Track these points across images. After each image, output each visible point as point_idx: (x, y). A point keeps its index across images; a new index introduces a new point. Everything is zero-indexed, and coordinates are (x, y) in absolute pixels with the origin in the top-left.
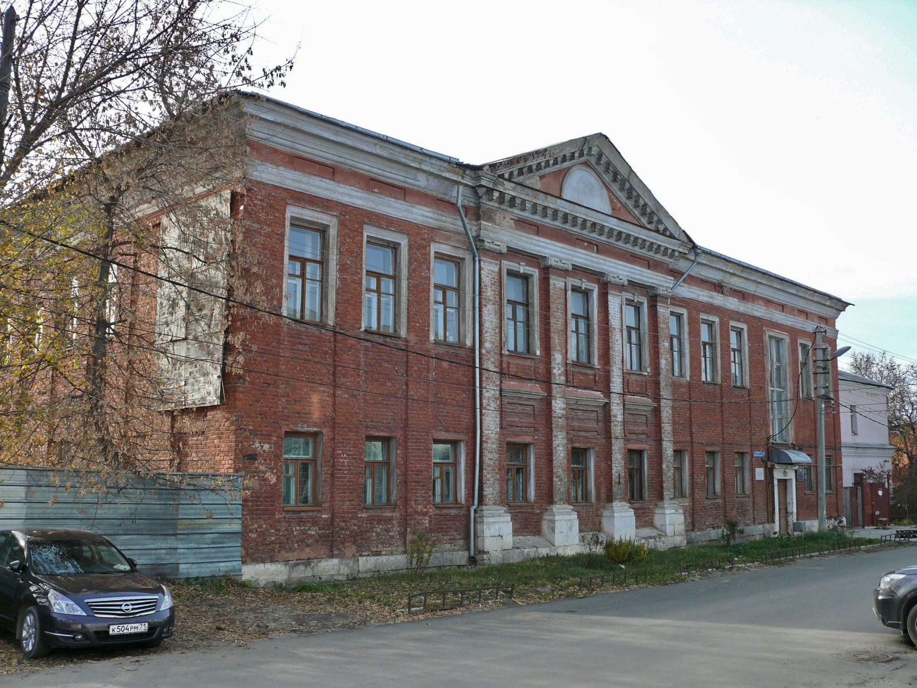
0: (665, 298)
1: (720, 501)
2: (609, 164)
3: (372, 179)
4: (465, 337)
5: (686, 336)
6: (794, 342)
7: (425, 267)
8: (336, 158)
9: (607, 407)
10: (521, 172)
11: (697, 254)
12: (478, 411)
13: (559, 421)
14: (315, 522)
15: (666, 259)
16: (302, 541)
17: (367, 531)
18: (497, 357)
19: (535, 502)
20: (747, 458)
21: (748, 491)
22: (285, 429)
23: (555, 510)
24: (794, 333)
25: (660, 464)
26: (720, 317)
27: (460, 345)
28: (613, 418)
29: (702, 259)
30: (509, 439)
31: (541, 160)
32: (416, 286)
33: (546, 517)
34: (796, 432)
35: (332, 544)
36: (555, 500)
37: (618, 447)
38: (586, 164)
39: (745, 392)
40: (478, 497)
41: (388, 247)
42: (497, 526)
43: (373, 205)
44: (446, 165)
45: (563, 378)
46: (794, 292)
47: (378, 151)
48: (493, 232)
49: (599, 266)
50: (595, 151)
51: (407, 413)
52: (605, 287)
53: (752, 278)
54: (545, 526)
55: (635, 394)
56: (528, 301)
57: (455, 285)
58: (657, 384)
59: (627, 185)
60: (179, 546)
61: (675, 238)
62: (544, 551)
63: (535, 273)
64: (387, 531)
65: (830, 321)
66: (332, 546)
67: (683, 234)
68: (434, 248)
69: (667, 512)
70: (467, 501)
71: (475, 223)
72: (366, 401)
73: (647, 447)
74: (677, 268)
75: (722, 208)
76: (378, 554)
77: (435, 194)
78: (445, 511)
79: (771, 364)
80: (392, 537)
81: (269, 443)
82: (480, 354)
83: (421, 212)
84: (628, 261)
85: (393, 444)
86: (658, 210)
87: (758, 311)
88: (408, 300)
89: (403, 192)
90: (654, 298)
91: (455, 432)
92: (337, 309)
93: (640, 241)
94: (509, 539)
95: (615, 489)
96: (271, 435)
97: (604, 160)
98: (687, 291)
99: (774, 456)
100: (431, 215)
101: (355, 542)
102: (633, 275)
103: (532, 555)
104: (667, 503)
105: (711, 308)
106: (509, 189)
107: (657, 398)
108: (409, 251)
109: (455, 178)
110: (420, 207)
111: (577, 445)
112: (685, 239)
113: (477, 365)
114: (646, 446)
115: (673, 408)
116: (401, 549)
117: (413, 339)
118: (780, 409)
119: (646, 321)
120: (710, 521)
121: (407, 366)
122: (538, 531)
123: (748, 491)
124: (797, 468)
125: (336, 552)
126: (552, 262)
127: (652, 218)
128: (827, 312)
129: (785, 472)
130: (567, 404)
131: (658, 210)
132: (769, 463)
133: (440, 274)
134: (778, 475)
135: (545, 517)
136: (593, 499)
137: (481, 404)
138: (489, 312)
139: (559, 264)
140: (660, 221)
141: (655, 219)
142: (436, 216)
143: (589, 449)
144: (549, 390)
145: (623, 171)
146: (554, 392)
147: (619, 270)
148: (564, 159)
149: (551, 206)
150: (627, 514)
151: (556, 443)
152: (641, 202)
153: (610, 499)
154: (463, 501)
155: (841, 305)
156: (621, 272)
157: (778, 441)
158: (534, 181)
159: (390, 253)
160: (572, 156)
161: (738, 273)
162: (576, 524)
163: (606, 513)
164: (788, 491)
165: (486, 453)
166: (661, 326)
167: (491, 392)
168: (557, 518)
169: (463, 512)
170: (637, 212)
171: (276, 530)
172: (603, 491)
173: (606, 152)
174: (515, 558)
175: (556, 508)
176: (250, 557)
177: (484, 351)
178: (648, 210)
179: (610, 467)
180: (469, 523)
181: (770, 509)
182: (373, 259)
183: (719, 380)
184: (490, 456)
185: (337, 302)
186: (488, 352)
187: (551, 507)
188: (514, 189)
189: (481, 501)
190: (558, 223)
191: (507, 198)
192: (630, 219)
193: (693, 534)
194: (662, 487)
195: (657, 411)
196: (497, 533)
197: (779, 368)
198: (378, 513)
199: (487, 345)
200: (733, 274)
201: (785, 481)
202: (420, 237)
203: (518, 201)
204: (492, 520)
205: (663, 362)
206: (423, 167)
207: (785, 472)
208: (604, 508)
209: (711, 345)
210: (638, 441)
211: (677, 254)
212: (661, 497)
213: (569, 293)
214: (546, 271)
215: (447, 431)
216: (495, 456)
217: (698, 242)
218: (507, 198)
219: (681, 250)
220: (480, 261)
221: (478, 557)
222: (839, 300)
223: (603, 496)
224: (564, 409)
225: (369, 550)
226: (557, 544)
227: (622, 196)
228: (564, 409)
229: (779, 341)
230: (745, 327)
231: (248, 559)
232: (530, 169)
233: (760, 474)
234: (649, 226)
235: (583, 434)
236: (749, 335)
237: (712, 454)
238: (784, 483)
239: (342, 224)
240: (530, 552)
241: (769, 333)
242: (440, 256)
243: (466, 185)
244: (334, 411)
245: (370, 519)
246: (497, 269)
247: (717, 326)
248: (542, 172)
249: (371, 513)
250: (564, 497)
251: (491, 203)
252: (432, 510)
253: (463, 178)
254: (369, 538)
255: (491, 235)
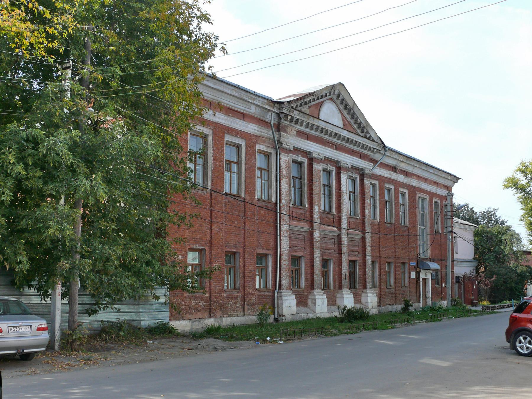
0: (368, 175)
1: (393, 290)
2: (343, 100)
3: (229, 109)
4: (272, 196)
5: (377, 197)
6: (431, 200)
7: (253, 158)
8: (212, 97)
9: (339, 236)
10: (301, 105)
11: (386, 151)
12: (279, 237)
13: (317, 244)
14: (202, 299)
15: (369, 153)
16: (196, 308)
17: (226, 304)
18: (288, 208)
19: (305, 289)
20: (407, 266)
21: (407, 285)
22: (188, 247)
23: (315, 293)
24: (432, 195)
25: (365, 268)
26: (394, 186)
27: (269, 201)
28: (342, 243)
29: (388, 153)
30: (292, 254)
31: (311, 98)
32: (249, 168)
33: (310, 297)
34: (432, 252)
35: (210, 311)
36: (315, 287)
37: (345, 259)
38: (331, 99)
39: (406, 229)
40: (277, 285)
41: (262, 154)
42: (289, 301)
43: (229, 124)
44: (266, 101)
45: (319, 220)
46: (432, 171)
47: (234, 93)
48: (286, 138)
49: (337, 157)
50: (337, 92)
51: (245, 239)
52: (339, 169)
53: (412, 164)
54: (310, 302)
55: (352, 229)
56: (301, 176)
57: (266, 168)
58: (364, 224)
59: (352, 112)
60: (141, 310)
61: (375, 142)
62: (311, 316)
63: (305, 161)
64: (235, 303)
65: (449, 188)
66: (210, 312)
67: (379, 139)
68: (259, 147)
69: (369, 295)
70: (272, 287)
71: (277, 133)
72: (225, 232)
73: (358, 259)
74: (374, 158)
75: (401, 125)
76: (231, 316)
77: (258, 116)
78: (262, 293)
79: (419, 212)
80: (238, 307)
81: (181, 255)
82: (280, 207)
83: (252, 127)
84: (350, 154)
85: (237, 256)
86: (367, 126)
87: (414, 182)
88: (245, 176)
89: (243, 116)
90: (363, 175)
91: (267, 249)
92: (212, 181)
93: (358, 143)
94: (294, 309)
95: (343, 282)
96: (181, 250)
97: (341, 98)
98: (380, 171)
99: (420, 265)
100: (259, 129)
101: (221, 310)
102: (353, 162)
103: (305, 318)
104: (368, 290)
105: (390, 181)
106: (296, 115)
107: (364, 232)
108: (246, 149)
109: (269, 108)
110: (251, 124)
111: (325, 257)
112: (380, 142)
113: (278, 211)
114: (358, 259)
115: (372, 237)
116: (242, 313)
117: (248, 198)
118: (423, 239)
119: (359, 188)
120: (388, 301)
121: (245, 213)
122: (306, 305)
123: (407, 285)
124: (432, 272)
125: (212, 315)
126: (315, 155)
127: (364, 130)
128: (448, 183)
129: (426, 274)
130: (321, 234)
131: (367, 126)
132: (418, 269)
133: (259, 161)
134: (422, 276)
135: (310, 297)
136: (332, 288)
137: (280, 234)
138: (284, 182)
139: (318, 156)
140: (367, 132)
141: (365, 130)
142: (259, 129)
143: (330, 259)
144: (312, 226)
145: (350, 104)
146: (315, 228)
147: (347, 160)
148: (322, 97)
149: (316, 124)
150: (349, 296)
151: (315, 256)
152: (359, 121)
153: (341, 287)
154: (270, 288)
155: (457, 179)
156: (347, 161)
157: (422, 257)
158: (306, 109)
159: (234, 149)
160: (326, 96)
161: (404, 161)
162: (326, 300)
163: (339, 295)
164: (427, 285)
165: (282, 261)
166: (366, 191)
167: (285, 227)
168: (317, 297)
169: (271, 294)
170: (355, 127)
171: (185, 303)
172: (337, 283)
173: (343, 93)
174: (298, 318)
175: (316, 292)
176: (173, 317)
177: (281, 205)
178: (362, 126)
179: (341, 270)
180: (274, 300)
181: (418, 295)
182: (229, 154)
183: (393, 221)
184: (284, 263)
185: (212, 177)
186: (283, 205)
187: (313, 291)
188: (298, 115)
189: (280, 288)
190: (318, 133)
191: (295, 119)
192: (352, 130)
193: (380, 308)
194: (366, 281)
195: (363, 239)
196: (289, 305)
197: (423, 215)
198: (231, 294)
199: (283, 201)
200: (402, 162)
201: (425, 279)
202: (251, 140)
203: (300, 121)
204: (286, 298)
205: (367, 211)
206: (255, 102)
207: (426, 274)
208: (338, 292)
209: (389, 202)
210: (354, 256)
211: (375, 150)
212: (365, 287)
213: (322, 172)
214: (311, 160)
215: (263, 249)
216: (287, 263)
217: (386, 144)
218: (295, 119)
219: (378, 148)
220: (280, 154)
221: (279, 318)
222: (455, 176)
223: (337, 286)
224: (319, 237)
225: (227, 314)
226: (316, 312)
227: (348, 117)
228: (319, 237)
229: (423, 200)
230: (406, 191)
231: (172, 319)
232: (306, 103)
233: (413, 275)
234: (361, 134)
235: (327, 251)
236: (409, 196)
237: (389, 263)
238: (425, 280)
239: (214, 134)
240: (304, 316)
241: (419, 195)
242: (260, 152)
243: (274, 112)
244: (211, 237)
245: (228, 297)
246: (288, 159)
247: (377, 186)
248: (310, 104)
249: (228, 293)
250: (319, 286)
251: (286, 122)
252: (256, 292)
253: (273, 108)
254: (227, 307)
255: (286, 140)
